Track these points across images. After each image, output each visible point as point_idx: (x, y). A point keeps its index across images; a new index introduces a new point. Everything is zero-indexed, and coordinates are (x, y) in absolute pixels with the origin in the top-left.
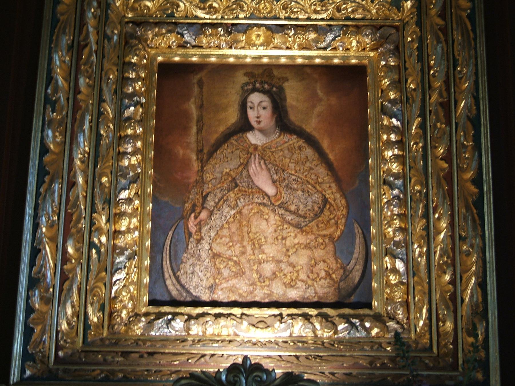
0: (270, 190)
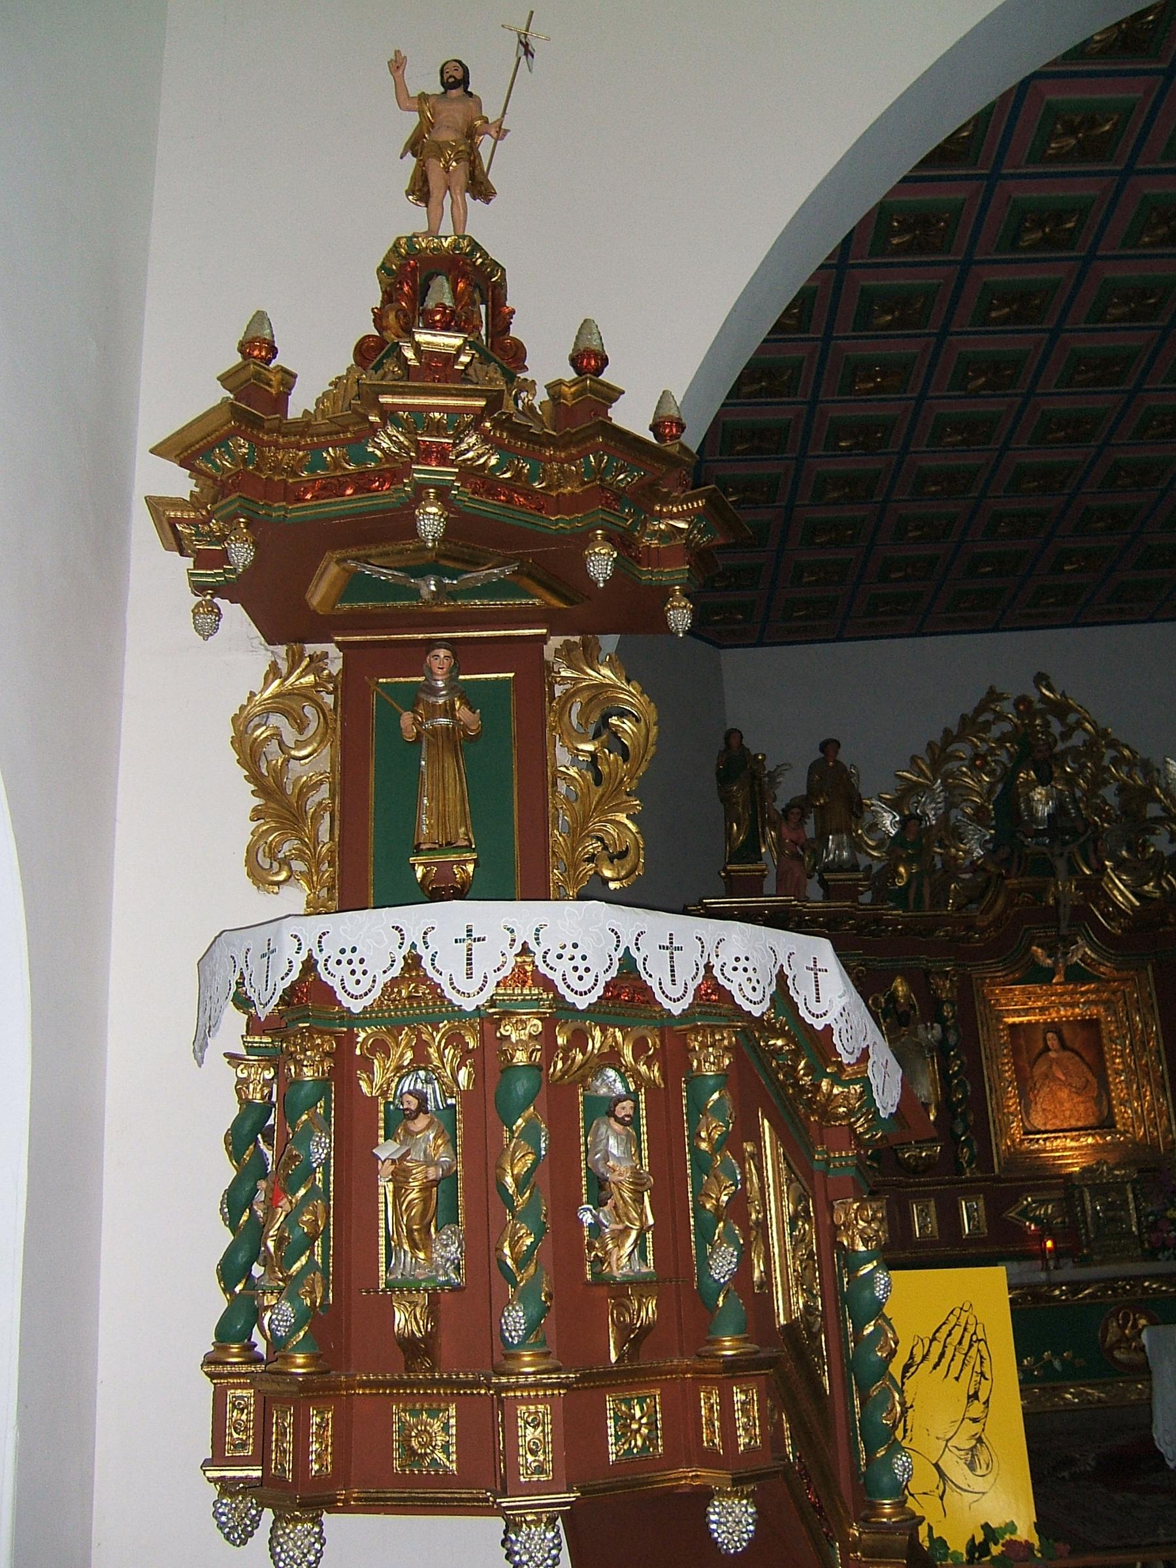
0: (1063, 1078)
